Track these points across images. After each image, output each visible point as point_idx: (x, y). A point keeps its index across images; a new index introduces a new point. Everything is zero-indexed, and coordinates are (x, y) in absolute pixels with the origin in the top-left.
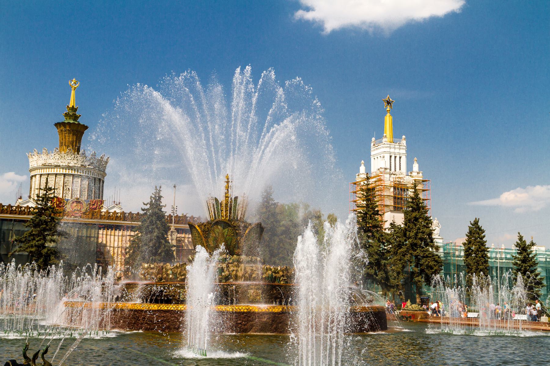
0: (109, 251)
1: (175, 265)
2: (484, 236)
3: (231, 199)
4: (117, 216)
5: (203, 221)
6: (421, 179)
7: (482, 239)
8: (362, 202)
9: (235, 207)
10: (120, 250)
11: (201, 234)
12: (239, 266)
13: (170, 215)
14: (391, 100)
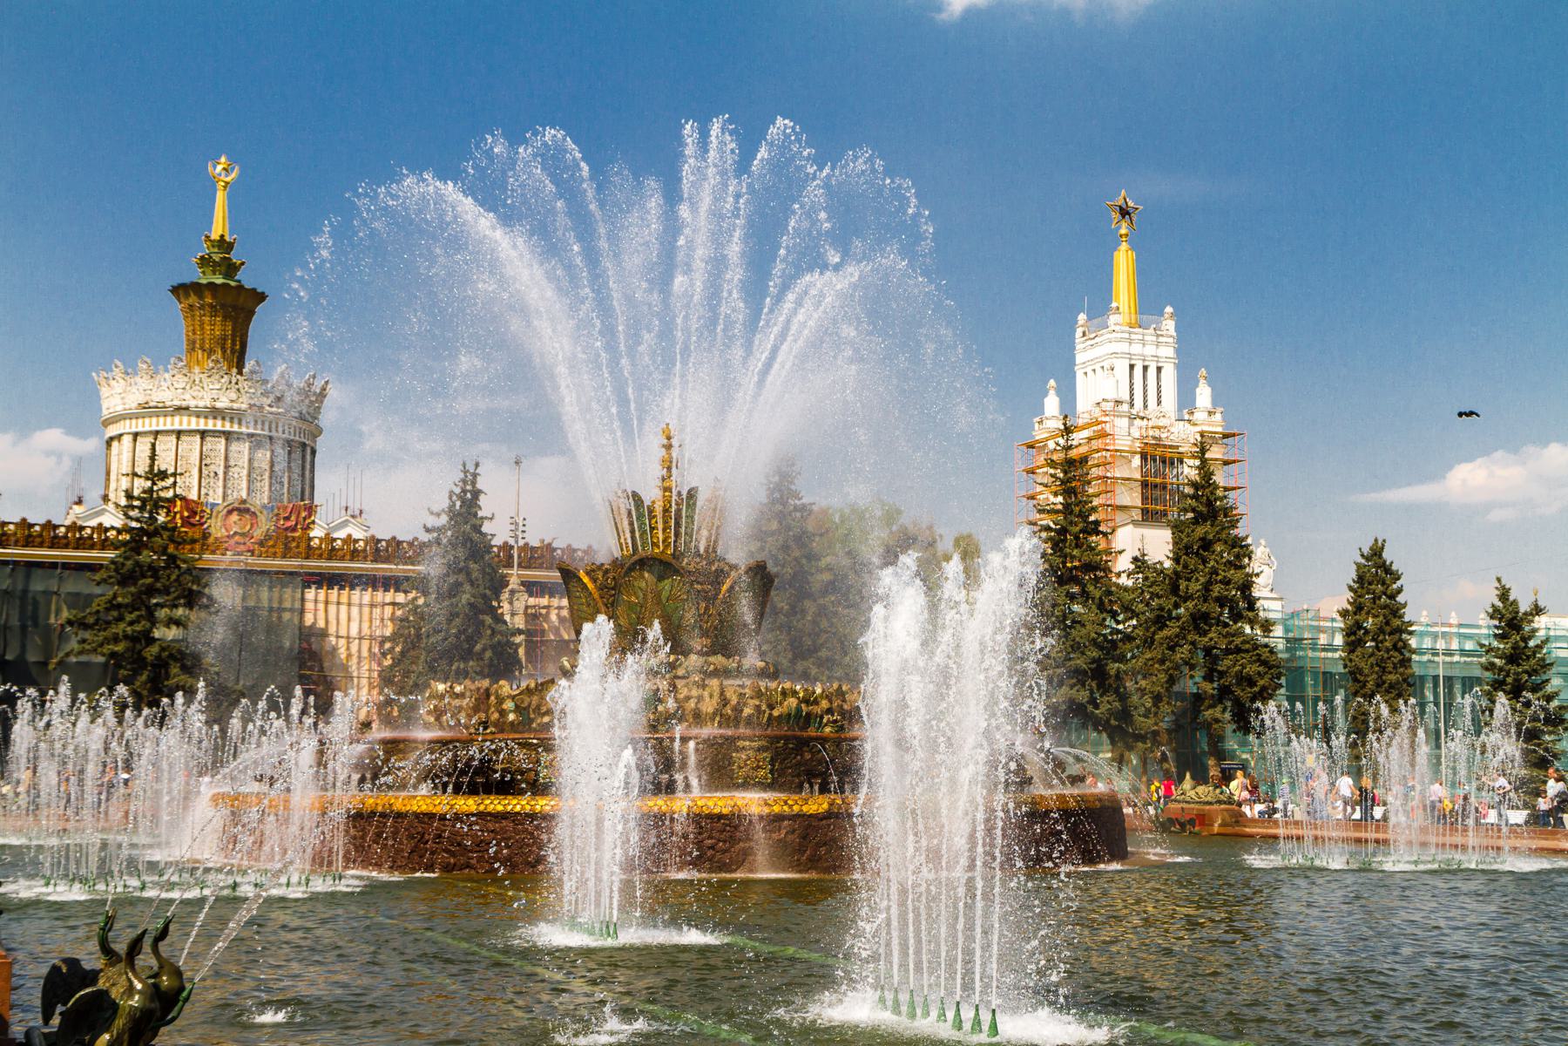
0: (335, 649)
1: (524, 685)
2: (1399, 591)
3: (679, 494)
4: (356, 550)
5: (603, 558)
6: (1220, 429)
7: (1392, 597)
8: (1052, 499)
9: (691, 518)
10: (366, 644)
11: (596, 596)
12: (704, 687)
13: (506, 543)
14: (1131, 204)
